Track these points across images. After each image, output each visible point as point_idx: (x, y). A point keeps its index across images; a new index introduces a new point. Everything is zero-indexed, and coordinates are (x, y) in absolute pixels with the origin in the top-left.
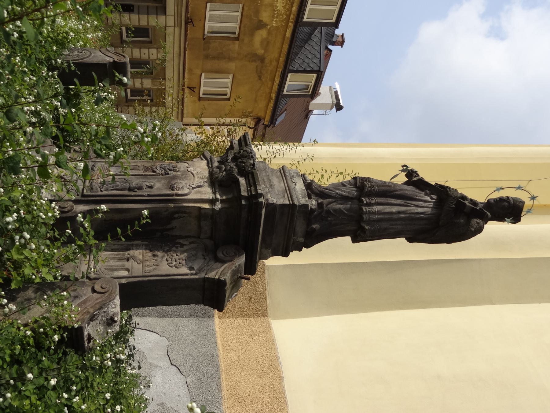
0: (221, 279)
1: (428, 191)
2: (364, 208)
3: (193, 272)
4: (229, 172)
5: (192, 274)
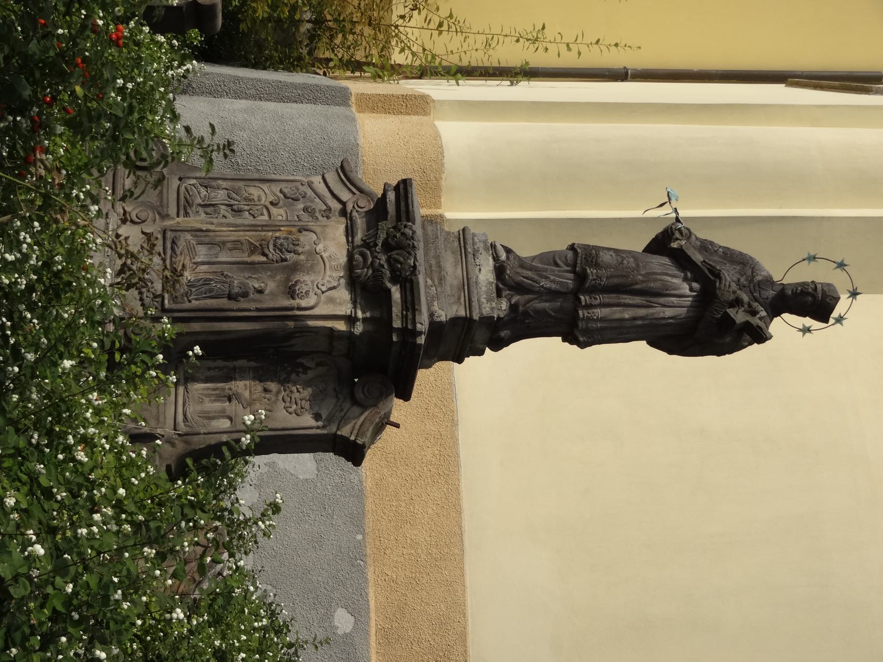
1: (689, 274)
2: (580, 312)
3: (320, 423)
4: (377, 271)
5: (318, 428)
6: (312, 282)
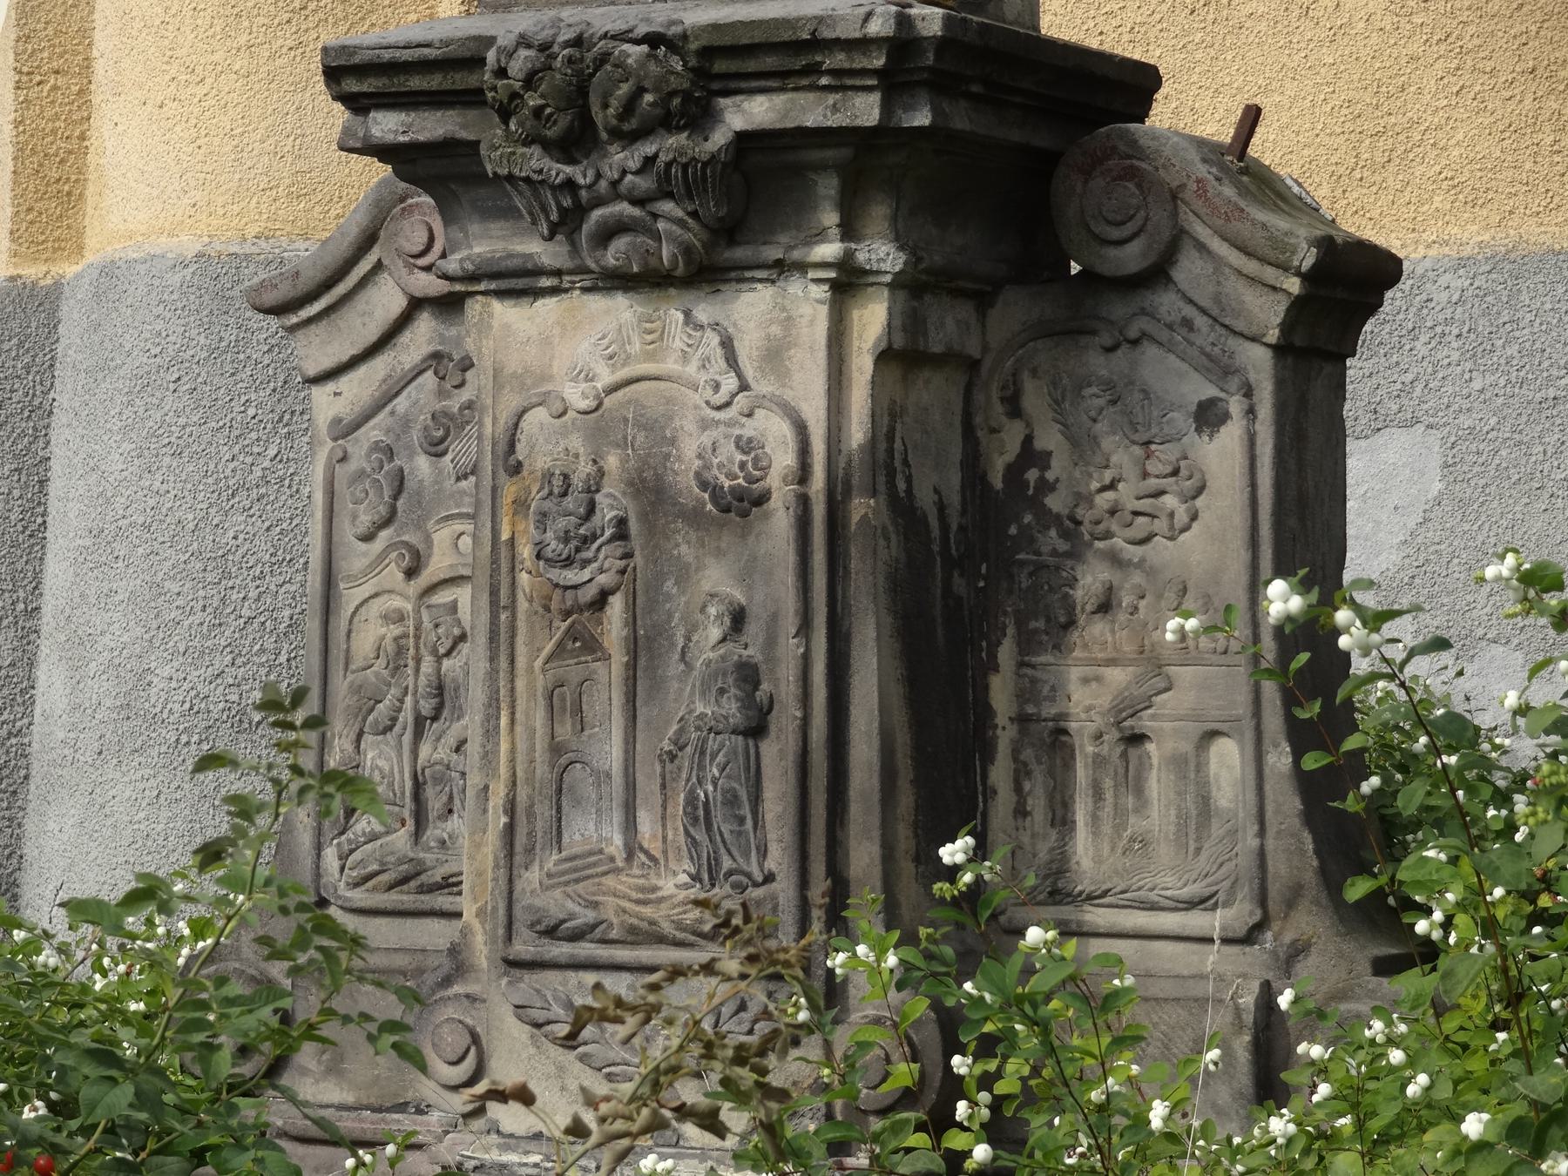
0: (1307, 264)
3: (1235, 406)
5: (1251, 412)
6: (705, 425)
